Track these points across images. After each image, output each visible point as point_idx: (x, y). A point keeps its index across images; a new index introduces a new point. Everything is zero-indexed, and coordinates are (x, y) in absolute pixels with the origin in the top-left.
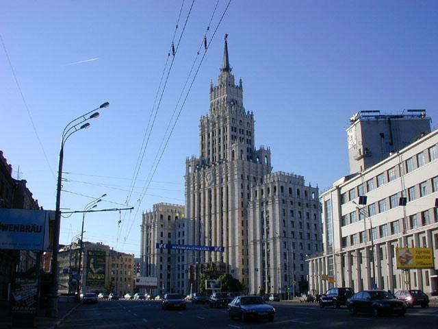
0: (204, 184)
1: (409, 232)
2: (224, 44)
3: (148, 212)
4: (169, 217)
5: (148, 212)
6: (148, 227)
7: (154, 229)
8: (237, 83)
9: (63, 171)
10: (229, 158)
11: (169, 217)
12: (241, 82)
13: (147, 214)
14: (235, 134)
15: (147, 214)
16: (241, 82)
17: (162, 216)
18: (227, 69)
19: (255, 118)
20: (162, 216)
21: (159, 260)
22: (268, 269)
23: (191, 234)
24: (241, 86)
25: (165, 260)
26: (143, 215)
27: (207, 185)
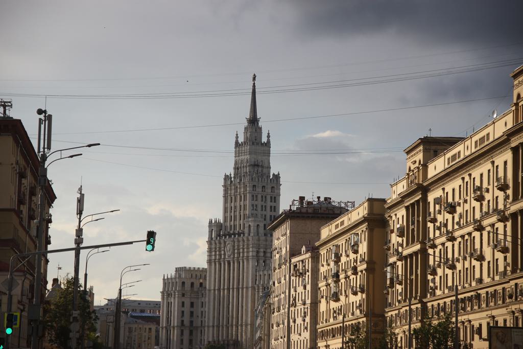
0: (225, 254)
1: (407, 308)
2: (250, 96)
3: (169, 277)
4: (192, 284)
5: (169, 277)
6: (169, 295)
7: (174, 298)
8: (264, 139)
9: (122, 295)
10: (246, 230)
11: (192, 284)
12: (268, 136)
13: (168, 278)
14: (256, 203)
15: (168, 278)
16: (268, 136)
17: (183, 283)
18: (253, 121)
19: (282, 181)
20: (183, 283)
21: (180, 333)
22: (238, 332)
23: (212, 304)
24: (269, 142)
25: (187, 332)
26: (164, 279)
27: (227, 257)
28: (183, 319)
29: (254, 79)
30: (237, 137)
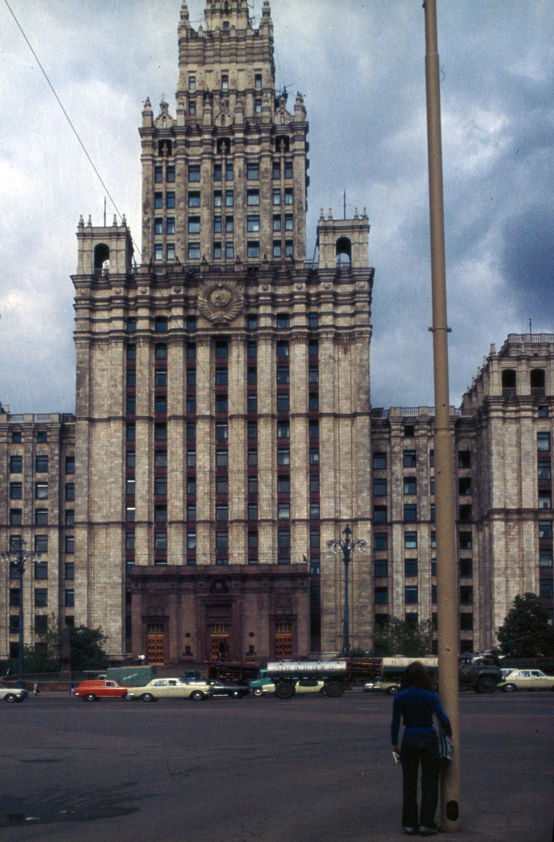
30: (185, 17)
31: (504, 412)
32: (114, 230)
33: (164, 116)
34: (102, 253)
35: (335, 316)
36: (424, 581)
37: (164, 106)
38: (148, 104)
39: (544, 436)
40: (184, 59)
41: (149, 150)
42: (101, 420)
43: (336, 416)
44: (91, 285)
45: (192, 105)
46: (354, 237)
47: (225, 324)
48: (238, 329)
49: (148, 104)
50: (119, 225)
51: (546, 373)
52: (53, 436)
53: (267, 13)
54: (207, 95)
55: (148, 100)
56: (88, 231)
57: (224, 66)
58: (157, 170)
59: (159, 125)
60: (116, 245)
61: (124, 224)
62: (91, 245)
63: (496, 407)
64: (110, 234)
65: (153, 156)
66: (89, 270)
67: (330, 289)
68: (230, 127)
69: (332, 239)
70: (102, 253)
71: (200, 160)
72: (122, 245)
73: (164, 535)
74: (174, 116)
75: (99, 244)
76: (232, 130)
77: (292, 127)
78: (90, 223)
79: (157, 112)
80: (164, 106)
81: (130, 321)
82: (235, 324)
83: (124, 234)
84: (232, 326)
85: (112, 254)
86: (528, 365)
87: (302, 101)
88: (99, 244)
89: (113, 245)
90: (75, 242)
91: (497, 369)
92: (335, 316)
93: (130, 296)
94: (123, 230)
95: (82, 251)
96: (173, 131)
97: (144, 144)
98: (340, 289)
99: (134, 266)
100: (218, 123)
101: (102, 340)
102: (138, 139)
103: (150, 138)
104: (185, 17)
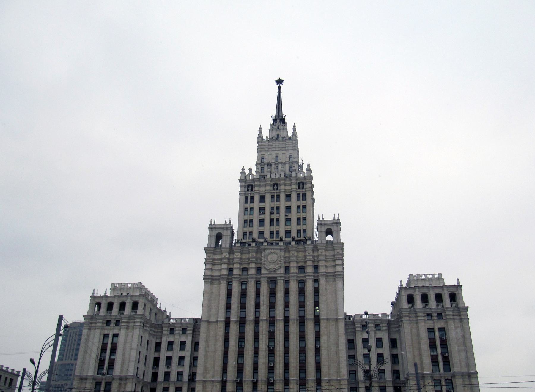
28: (396, 368)
29: (280, 82)
30: (260, 132)
31: (410, 317)
32: (225, 226)
33: (250, 173)
34: (219, 237)
35: (326, 266)
36: (175, 369)
37: (250, 170)
38: (243, 169)
39: (431, 330)
40: (260, 150)
41: (243, 189)
42: (213, 322)
43: (328, 320)
44: (213, 251)
45: (262, 169)
46: (334, 228)
47: (274, 271)
48: (280, 274)
49: (243, 169)
50: (228, 223)
51: (414, 296)
52: (190, 331)
53: (294, 129)
54: (269, 164)
55: (243, 167)
56: (214, 226)
57: (276, 152)
58: (247, 198)
59: (247, 178)
60: (226, 234)
61: (230, 222)
62: (215, 233)
63: (421, 314)
64: (223, 228)
65: (244, 191)
66: (213, 245)
67: (324, 253)
68: (278, 178)
69: (324, 229)
70: (219, 237)
71: (265, 193)
72: (229, 233)
73: (241, 388)
74: (255, 174)
75: (218, 233)
76: (279, 179)
77: (305, 178)
78: (215, 223)
79: (247, 172)
80: (250, 170)
81: (230, 270)
82: (278, 272)
83: (229, 228)
84: (278, 272)
85: (224, 237)
86: (106, 300)
87: (310, 166)
88: (218, 233)
89: (224, 233)
90: (207, 232)
91: (404, 294)
92: (326, 266)
93: (231, 257)
94: (229, 226)
95: (210, 236)
96: (254, 180)
97: (241, 186)
98: (327, 253)
99: (220, 247)
100: (273, 177)
101: (216, 279)
102: (239, 184)
103: (244, 184)
104: (260, 132)
